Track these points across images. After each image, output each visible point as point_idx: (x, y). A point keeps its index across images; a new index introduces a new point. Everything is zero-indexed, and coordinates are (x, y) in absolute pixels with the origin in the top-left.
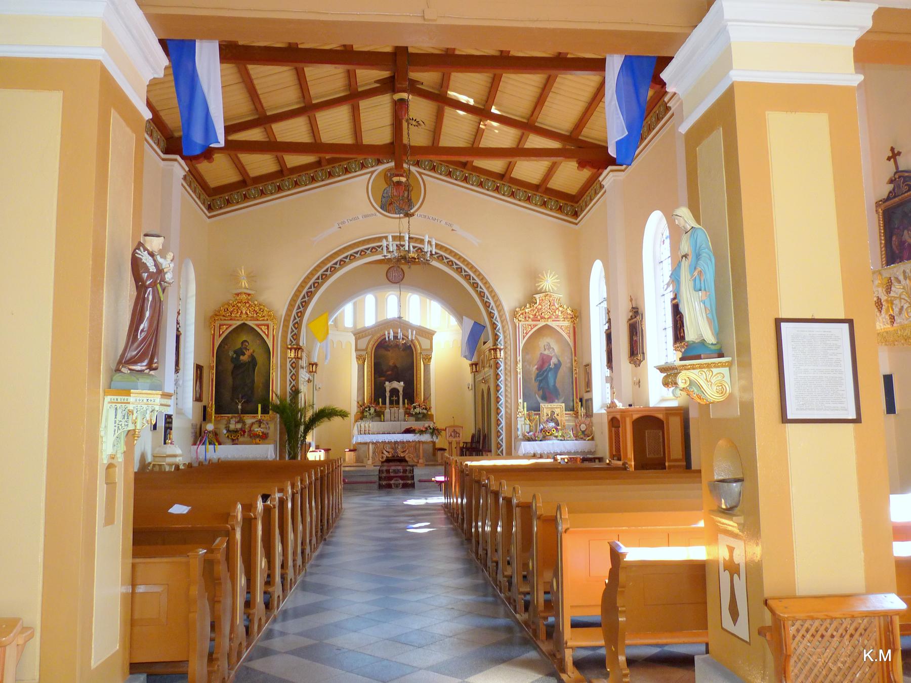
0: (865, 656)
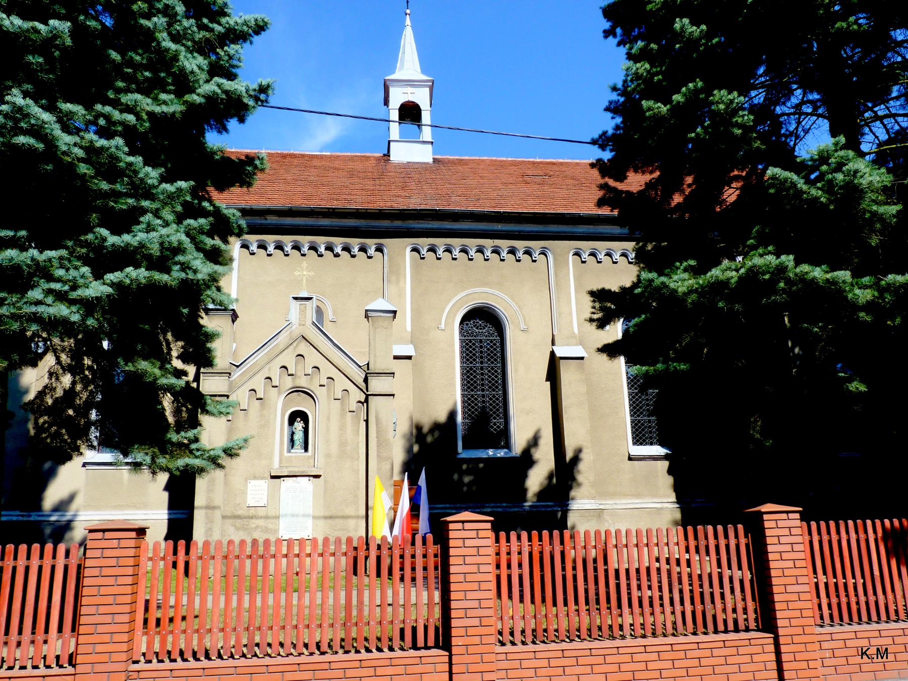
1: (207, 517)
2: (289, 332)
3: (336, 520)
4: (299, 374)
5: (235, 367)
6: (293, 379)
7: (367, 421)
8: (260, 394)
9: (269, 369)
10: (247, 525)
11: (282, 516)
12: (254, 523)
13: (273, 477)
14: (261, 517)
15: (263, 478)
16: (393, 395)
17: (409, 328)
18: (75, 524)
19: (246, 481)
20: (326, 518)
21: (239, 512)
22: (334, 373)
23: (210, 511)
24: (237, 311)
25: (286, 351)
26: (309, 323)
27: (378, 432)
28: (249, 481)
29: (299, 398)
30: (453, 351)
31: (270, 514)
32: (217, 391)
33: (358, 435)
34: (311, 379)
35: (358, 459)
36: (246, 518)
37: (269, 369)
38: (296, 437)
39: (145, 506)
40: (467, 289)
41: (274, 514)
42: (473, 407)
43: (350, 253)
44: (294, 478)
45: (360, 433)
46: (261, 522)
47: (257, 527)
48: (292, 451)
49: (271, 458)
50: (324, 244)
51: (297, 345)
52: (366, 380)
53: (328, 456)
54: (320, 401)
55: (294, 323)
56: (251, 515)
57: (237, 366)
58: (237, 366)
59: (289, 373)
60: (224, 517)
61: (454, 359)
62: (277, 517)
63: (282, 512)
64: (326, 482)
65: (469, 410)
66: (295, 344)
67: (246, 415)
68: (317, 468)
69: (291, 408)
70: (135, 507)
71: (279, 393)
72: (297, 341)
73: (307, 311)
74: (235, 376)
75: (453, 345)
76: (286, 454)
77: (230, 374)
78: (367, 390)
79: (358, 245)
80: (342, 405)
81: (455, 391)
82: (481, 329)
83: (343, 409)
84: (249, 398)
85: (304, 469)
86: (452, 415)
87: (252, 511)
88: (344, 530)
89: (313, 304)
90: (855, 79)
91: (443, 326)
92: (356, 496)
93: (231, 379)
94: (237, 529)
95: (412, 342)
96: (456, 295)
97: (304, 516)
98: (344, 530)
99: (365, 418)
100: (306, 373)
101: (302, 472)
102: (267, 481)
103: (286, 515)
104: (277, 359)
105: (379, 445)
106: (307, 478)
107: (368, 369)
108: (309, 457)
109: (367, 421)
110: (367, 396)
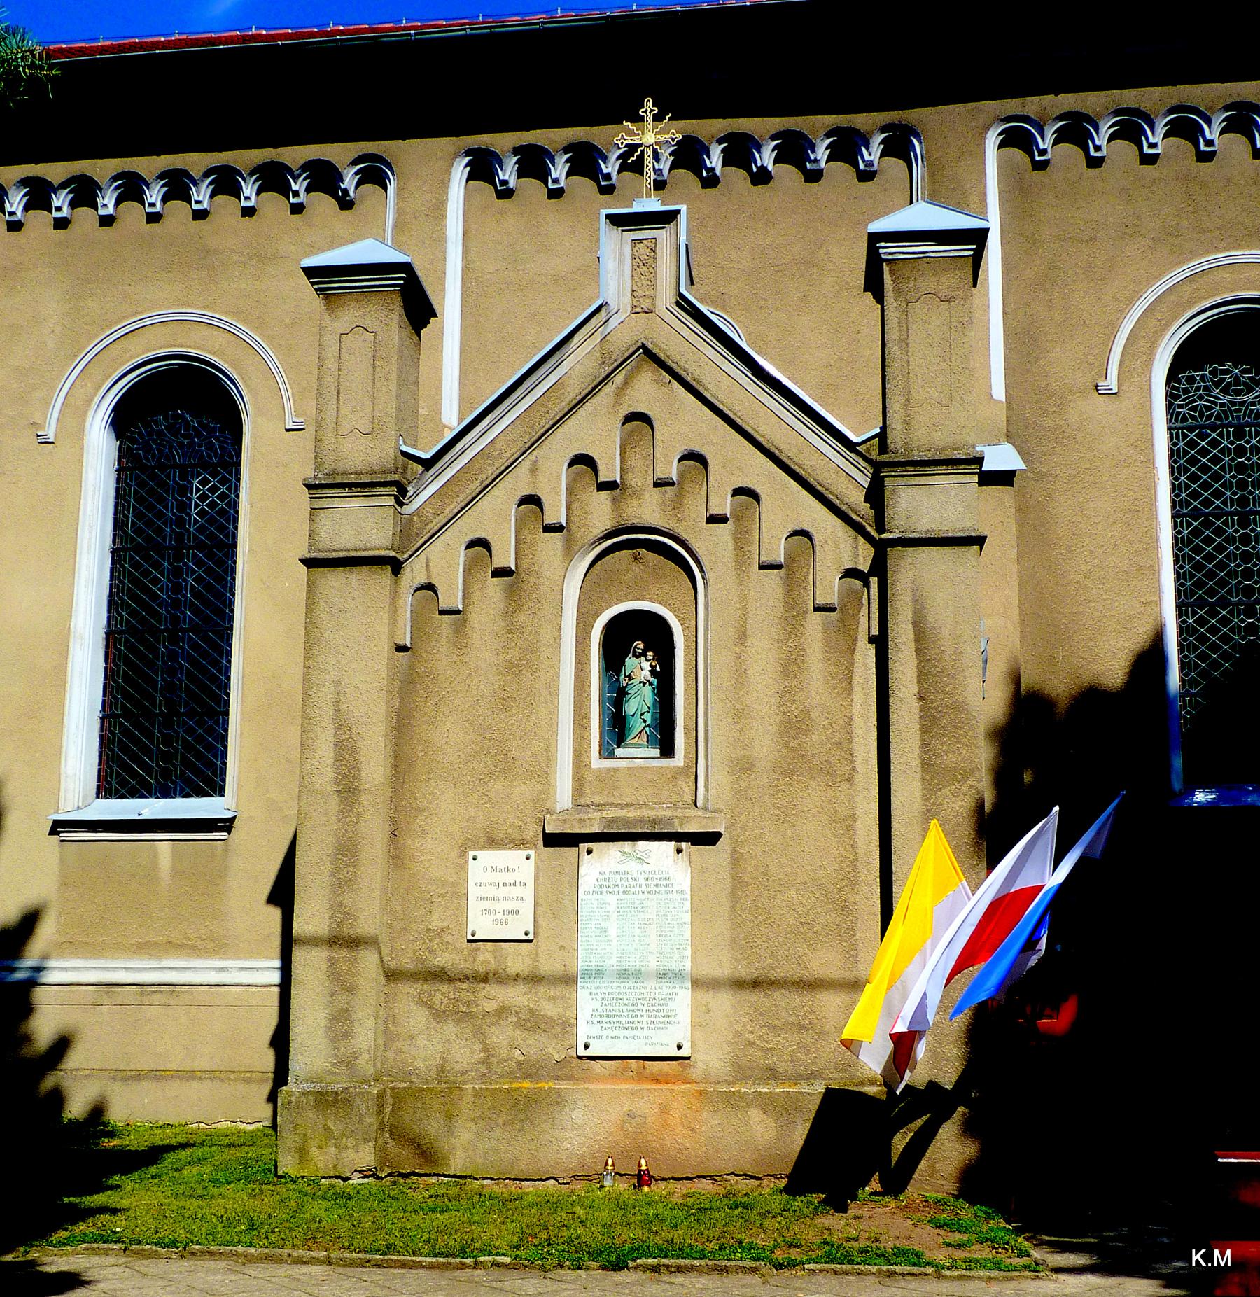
0: (1194, 1258)
1: (335, 974)
2: (597, 338)
3: (777, 994)
4: (634, 481)
5: (420, 469)
6: (615, 501)
7: (881, 642)
8: (505, 557)
9: (533, 471)
10: (469, 1003)
11: (588, 974)
12: (492, 997)
13: (552, 840)
14: (516, 978)
15: (518, 845)
16: (979, 541)
17: (999, 392)
18: (40, 995)
19: (463, 853)
20: (739, 984)
21: (444, 960)
22: (760, 472)
23: (344, 953)
24: (420, 273)
25: (589, 406)
26: (665, 300)
27: (922, 677)
28: (472, 854)
29: (635, 567)
30: (1150, 463)
31: (547, 967)
32: (357, 544)
33: (850, 692)
34: (679, 497)
35: (850, 780)
36: (465, 978)
37: (533, 471)
38: (630, 707)
39: (217, 946)
40: (1193, 254)
41: (560, 969)
42: (1214, 648)
43: (802, 168)
44: (627, 846)
45: (856, 688)
46: (516, 995)
47: (501, 1012)
48: (619, 752)
49: (543, 773)
50: (720, 141)
51: (626, 382)
52: (876, 495)
53: (743, 767)
54: (709, 574)
55: (613, 306)
56: (481, 969)
57: (428, 464)
58: (428, 464)
59: (602, 478)
60: (391, 975)
61: (1152, 487)
62: (570, 980)
63: (586, 960)
64: (736, 857)
65: (1203, 657)
66: (619, 379)
67: (459, 631)
68: (706, 808)
69: (610, 605)
70: (190, 948)
71: (570, 552)
72: (628, 367)
73: (660, 264)
74: (420, 498)
75: (1149, 442)
76: (597, 763)
77: (402, 491)
78: (881, 528)
79: (828, 136)
80: (790, 584)
81: (1158, 591)
82: (1238, 393)
83: (791, 602)
84: (468, 573)
85: (660, 814)
86: (1151, 658)
87: (485, 959)
88: (803, 1028)
89: (678, 234)
90: (1027, 777)
91: (1112, 381)
92: (845, 909)
93: (407, 510)
94: (439, 1015)
95: (1009, 438)
96: (1157, 278)
97: (661, 976)
98: (803, 1028)
99: (875, 631)
100: (660, 475)
101: (654, 822)
102: (532, 853)
103: (599, 973)
104: (560, 433)
105: (929, 724)
106: (670, 846)
107: (883, 448)
108: (677, 773)
109: (881, 642)
110: (881, 549)
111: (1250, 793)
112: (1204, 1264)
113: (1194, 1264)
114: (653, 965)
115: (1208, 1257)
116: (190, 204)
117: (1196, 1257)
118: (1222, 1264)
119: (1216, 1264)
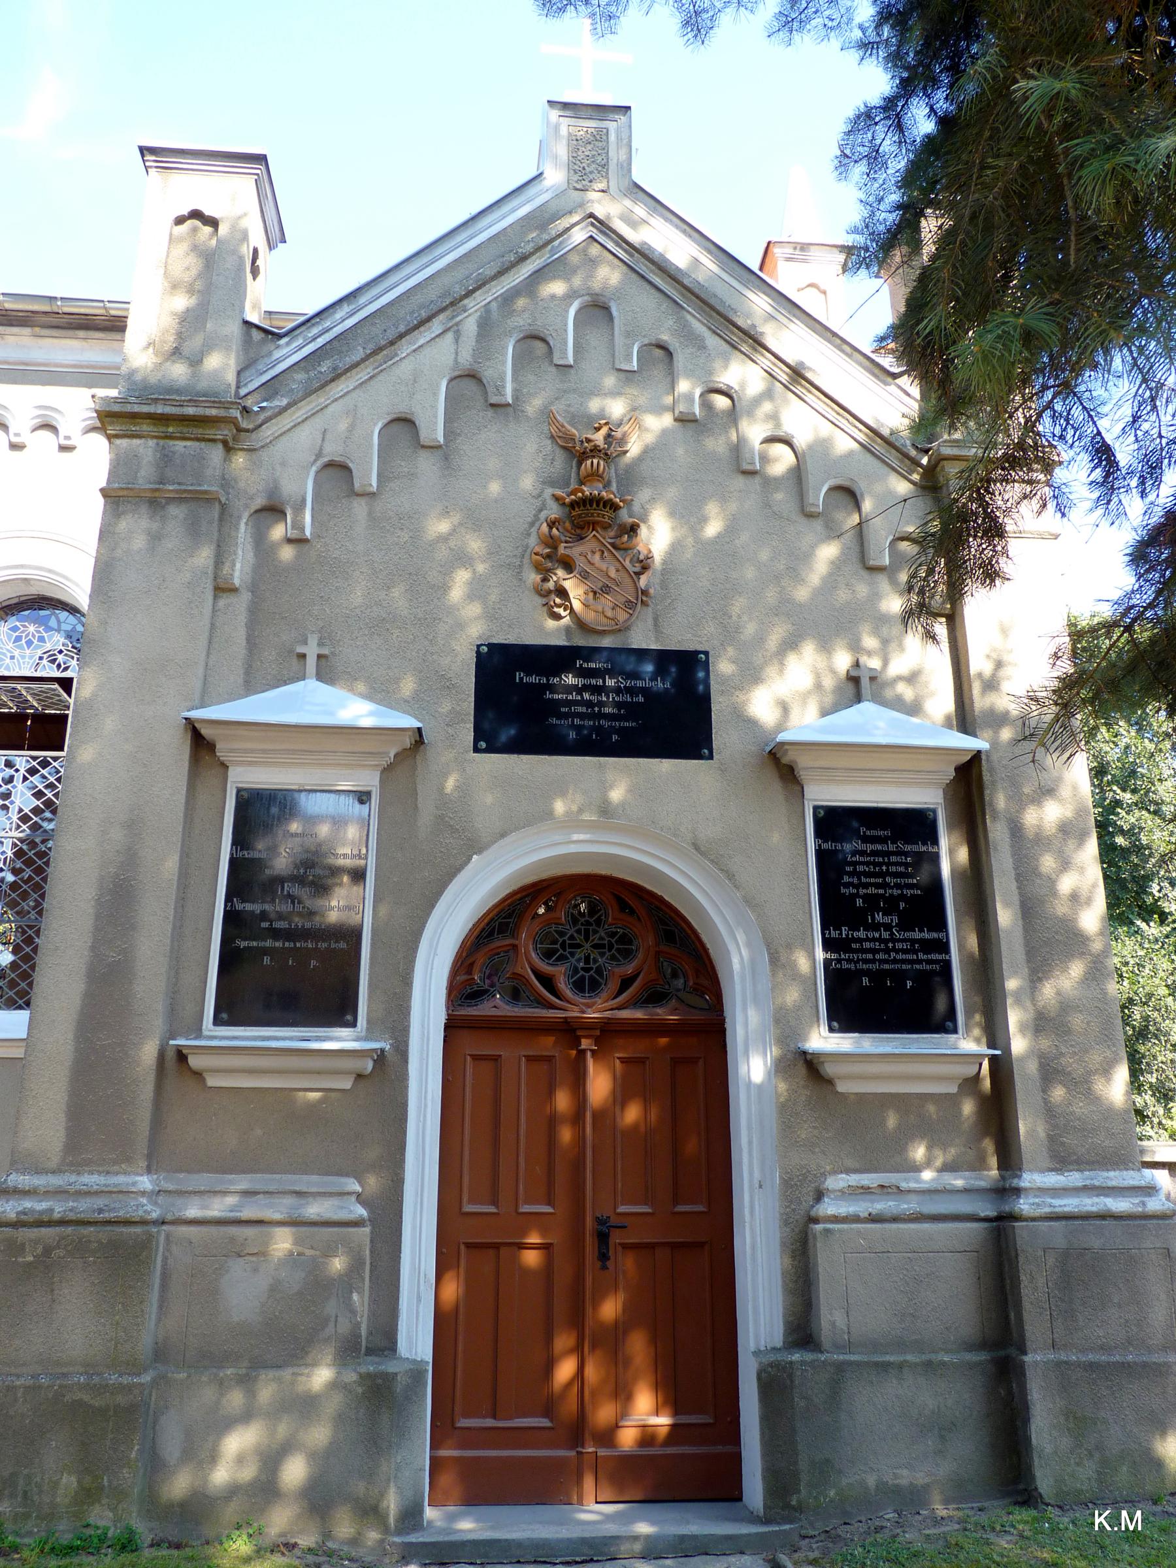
0: (1097, 1521)
19: (456, 1428)
111: (1037, 471)
112: (1109, 1528)
113: (1097, 1528)
114: (526, 526)
115: (1115, 1520)
116: (7, 433)
117: (1100, 1520)
118: (1131, 1528)
119: (1123, 1529)
